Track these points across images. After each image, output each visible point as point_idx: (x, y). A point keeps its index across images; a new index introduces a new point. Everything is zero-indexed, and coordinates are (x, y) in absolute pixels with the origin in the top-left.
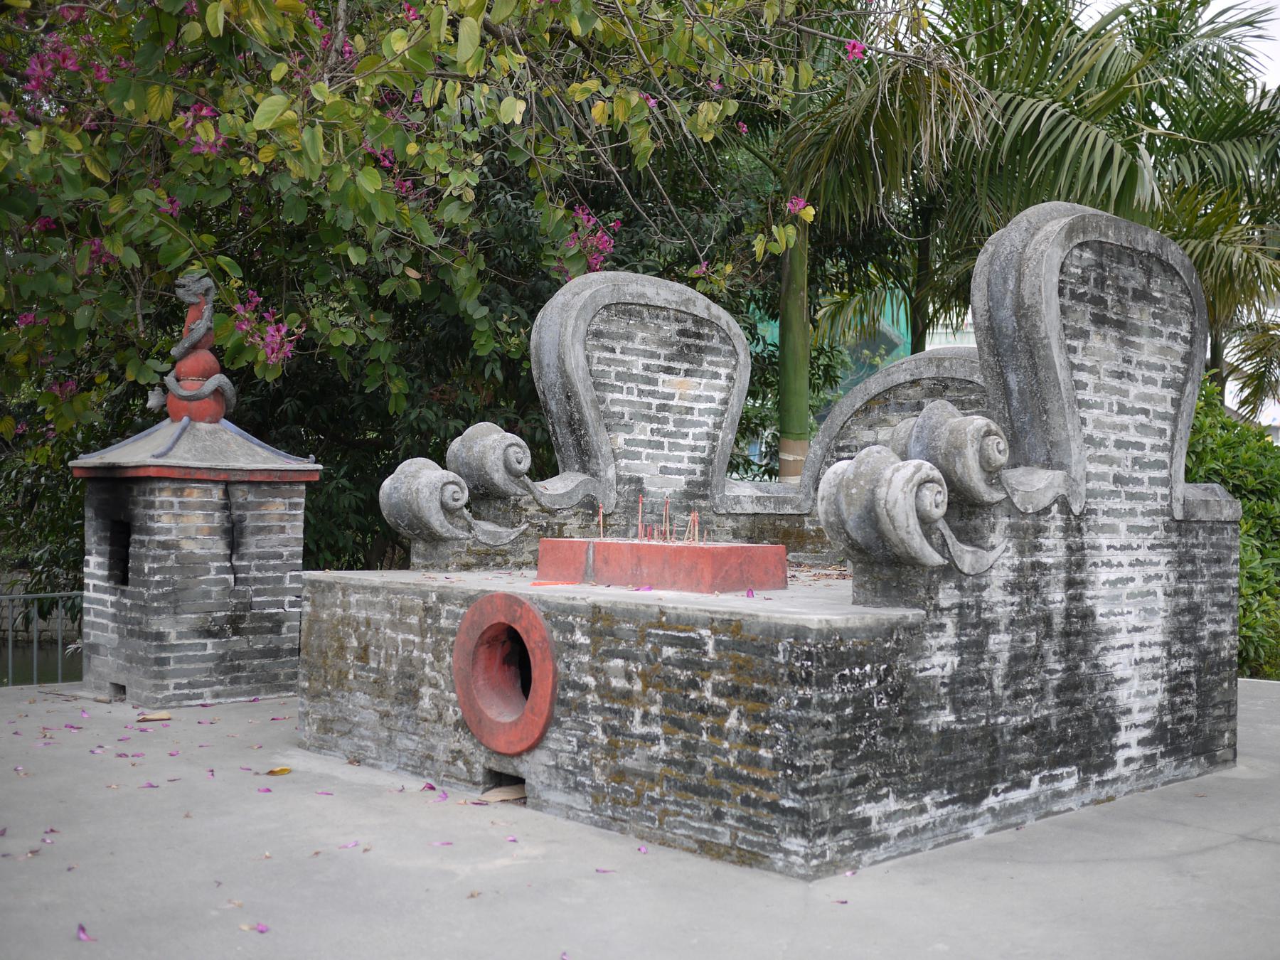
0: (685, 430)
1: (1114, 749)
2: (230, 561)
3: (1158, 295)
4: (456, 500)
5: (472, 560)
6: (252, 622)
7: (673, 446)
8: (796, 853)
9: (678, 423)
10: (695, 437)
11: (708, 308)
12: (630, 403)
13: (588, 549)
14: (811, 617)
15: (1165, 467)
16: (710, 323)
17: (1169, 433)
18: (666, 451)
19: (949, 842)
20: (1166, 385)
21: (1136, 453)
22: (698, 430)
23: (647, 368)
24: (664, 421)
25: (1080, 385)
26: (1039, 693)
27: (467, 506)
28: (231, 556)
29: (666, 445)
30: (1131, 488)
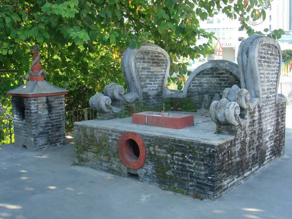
0: (157, 80)
1: (265, 157)
2: (49, 115)
3: (274, 54)
4: (109, 103)
5: (112, 117)
6: (46, 118)
7: (154, 84)
8: (211, 195)
9: (155, 78)
10: (159, 81)
11: (161, 50)
12: (145, 74)
13: (145, 117)
14: (215, 142)
15: (275, 93)
16: (161, 53)
17: (275, 85)
18: (153, 85)
19: (238, 185)
20: (275, 74)
21: (270, 91)
22: (159, 79)
23: (148, 66)
24: (152, 78)
25: (261, 78)
26: (253, 149)
27: (111, 104)
28: (49, 114)
29: (153, 84)
30: (270, 99)
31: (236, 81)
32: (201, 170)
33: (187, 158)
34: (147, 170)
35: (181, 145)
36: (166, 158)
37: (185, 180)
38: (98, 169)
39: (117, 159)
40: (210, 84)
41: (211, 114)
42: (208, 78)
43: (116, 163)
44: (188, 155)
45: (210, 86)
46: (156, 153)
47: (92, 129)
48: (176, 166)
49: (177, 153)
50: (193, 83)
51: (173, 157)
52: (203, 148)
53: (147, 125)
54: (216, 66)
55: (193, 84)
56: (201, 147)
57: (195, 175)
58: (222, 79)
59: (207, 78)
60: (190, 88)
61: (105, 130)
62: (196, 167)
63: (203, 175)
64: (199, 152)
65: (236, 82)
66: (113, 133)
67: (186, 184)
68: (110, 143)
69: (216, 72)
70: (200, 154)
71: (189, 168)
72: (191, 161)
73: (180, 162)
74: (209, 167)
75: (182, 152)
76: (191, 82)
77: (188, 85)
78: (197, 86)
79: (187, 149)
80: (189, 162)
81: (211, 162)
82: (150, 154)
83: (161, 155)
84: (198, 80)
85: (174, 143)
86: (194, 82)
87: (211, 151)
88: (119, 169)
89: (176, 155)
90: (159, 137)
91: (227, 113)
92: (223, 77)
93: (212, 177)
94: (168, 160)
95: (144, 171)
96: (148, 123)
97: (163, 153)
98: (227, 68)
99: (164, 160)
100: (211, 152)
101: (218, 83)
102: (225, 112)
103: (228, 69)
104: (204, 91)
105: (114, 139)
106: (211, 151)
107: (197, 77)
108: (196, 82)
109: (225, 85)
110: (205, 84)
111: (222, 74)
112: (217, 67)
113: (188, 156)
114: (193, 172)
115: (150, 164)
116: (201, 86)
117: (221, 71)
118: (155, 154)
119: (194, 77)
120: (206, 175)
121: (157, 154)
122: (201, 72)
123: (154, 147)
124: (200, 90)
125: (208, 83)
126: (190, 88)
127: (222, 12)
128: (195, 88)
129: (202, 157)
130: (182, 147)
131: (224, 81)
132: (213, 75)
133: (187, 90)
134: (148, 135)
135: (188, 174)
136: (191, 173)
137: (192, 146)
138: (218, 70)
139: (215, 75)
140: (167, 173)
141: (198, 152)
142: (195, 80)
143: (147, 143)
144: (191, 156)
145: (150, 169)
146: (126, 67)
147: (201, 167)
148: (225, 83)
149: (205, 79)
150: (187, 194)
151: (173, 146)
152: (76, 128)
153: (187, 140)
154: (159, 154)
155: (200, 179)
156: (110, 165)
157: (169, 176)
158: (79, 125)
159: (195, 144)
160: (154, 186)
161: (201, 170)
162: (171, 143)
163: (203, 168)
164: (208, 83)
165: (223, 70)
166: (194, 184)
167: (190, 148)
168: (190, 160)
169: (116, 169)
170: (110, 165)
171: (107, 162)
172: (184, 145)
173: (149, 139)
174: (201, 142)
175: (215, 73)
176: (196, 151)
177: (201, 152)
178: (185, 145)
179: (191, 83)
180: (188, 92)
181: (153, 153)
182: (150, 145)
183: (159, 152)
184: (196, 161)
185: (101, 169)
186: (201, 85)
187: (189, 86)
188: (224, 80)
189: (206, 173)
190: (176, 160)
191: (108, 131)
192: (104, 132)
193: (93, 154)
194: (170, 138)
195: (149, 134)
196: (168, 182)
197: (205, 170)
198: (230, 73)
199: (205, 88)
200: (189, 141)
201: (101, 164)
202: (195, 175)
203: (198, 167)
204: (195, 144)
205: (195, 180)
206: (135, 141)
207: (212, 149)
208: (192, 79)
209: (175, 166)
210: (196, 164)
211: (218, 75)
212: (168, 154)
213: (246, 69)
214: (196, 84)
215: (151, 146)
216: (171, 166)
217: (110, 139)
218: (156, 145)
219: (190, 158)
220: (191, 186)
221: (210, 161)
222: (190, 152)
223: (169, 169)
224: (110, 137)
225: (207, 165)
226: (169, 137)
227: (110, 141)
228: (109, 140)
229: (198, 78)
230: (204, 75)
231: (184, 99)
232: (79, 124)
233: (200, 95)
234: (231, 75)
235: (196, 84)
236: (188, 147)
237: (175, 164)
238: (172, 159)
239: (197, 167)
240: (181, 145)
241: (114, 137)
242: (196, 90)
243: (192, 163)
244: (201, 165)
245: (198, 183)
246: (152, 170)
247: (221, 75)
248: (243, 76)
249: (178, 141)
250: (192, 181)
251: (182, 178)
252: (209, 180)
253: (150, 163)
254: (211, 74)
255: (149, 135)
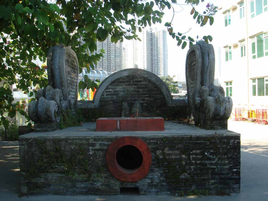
31: (155, 88)
32: (225, 165)
33: (207, 155)
34: (152, 179)
35: (199, 142)
36: (181, 159)
37: (204, 180)
38: (67, 193)
39: (102, 175)
40: (126, 92)
41: (211, 109)
42: (124, 86)
43: (103, 180)
44: (209, 151)
45: (127, 94)
46: (166, 157)
47: (56, 141)
48: (193, 166)
49: (194, 152)
50: (106, 92)
51: (189, 157)
52: (226, 141)
53: (120, 131)
54: (133, 74)
55: (106, 93)
56: (223, 140)
57: (217, 171)
58: (140, 86)
59: (123, 86)
60: (103, 97)
61: (81, 140)
62: (218, 163)
63: (226, 169)
64: (222, 146)
65: (155, 89)
66: (96, 142)
67: (207, 184)
68: (92, 155)
69: (133, 80)
70: (223, 148)
71: (210, 165)
72: (213, 157)
73: (198, 160)
74: (233, 159)
75: (201, 150)
76: (104, 91)
77: (101, 94)
78: (112, 95)
79: (207, 145)
80: (210, 159)
81: (236, 153)
82: (157, 158)
83: (173, 157)
84: (112, 89)
85: (191, 141)
86: (108, 90)
87: (236, 142)
88: (107, 187)
89: (193, 154)
90: (170, 137)
91: (228, 106)
92: (141, 85)
93: (237, 169)
94: (182, 162)
95: (148, 181)
96: (121, 128)
97: (176, 155)
98: (145, 76)
99: (177, 162)
100: (235, 144)
101: (135, 91)
102: (227, 106)
103: (147, 76)
104: (120, 99)
105: (98, 150)
106: (236, 142)
107: (112, 86)
108: (111, 90)
109: (143, 93)
110: (121, 92)
111: (140, 81)
112: (134, 75)
113: (209, 153)
114: (215, 169)
115: (157, 171)
116: (116, 95)
117: (139, 79)
118: (164, 157)
119: (108, 86)
120: (231, 169)
121: (167, 157)
122: (116, 80)
123: (163, 150)
124: (115, 99)
125: (124, 91)
126: (103, 97)
127: (194, 18)
128: (110, 97)
129: (225, 151)
130: (200, 144)
131: (141, 89)
132: (130, 83)
133: (99, 99)
134: (154, 137)
135: (209, 172)
136: (213, 170)
137: (213, 141)
138: (135, 78)
139: (132, 83)
140: (181, 177)
141: (220, 146)
142: (109, 89)
143: (152, 147)
144: (212, 152)
145: (156, 176)
146: (57, 69)
147: (224, 161)
148: (143, 91)
149: (121, 87)
150: (210, 194)
151: (190, 145)
152: (24, 143)
153: (207, 136)
154: (171, 157)
155: (224, 174)
156: (91, 184)
157: (183, 179)
158: (30, 139)
159: (217, 138)
160: (163, 195)
161: (225, 165)
162: (187, 141)
163: (226, 162)
164: (124, 91)
165: (140, 78)
166: (216, 181)
167: (211, 143)
168: (211, 156)
169: (101, 187)
170: (91, 184)
171: (86, 181)
172: (203, 141)
173: (155, 141)
174: (223, 135)
175: (132, 81)
176: (218, 146)
177: (224, 146)
178: (204, 142)
179: (105, 92)
180: (101, 101)
181: (161, 157)
182: (154, 150)
183: (169, 155)
184: (219, 156)
185: (74, 192)
186: (116, 93)
187: (102, 95)
188: (143, 88)
189: (231, 166)
190: (193, 160)
191: (88, 140)
192: (78, 142)
193: (59, 174)
194: (184, 136)
195: (155, 136)
196: (183, 187)
197: (229, 163)
198: (148, 80)
199: (121, 96)
200: (209, 136)
201: (74, 186)
202: (218, 170)
203: (221, 162)
204: (217, 138)
205: (217, 177)
206: (135, 146)
207: (236, 140)
208: (106, 87)
209: (192, 167)
210: (219, 159)
211: (135, 83)
212: (183, 154)
213: (207, 71)
214: (110, 93)
215: (158, 149)
216: (187, 167)
217: (91, 150)
218: (166, 147)
219: (211, 154)
220: (213, 184)
221: (235, 153)
222: (211, 148)
223: (184, 171)
224: (90, 148)
225: (231, 157)
226: (184, 135)
227: (91, 153)
228: (89, 152)
229: (113, 87)
230: (119, 84)
231: (95, 109)
232: (30, 138)
233: (115, 104)
234: (149, 82)
235: (110, 93)
236: (209, 142)
237: (192, 164)
238: (188, 160)
239: (220, 162)
240: (199, 142)
241: (97, 147)
242: (110, 99)
243: (214, 159)
244: (224, 159)
245: (221, 179)
246: (160, 177)
247: (139, 83)
248: (199, 78)
249: (195, 138)
250: (213, 179)
251: (202, 178)
252: (234, 172)
253: (157, 170)
254: (127, 82)
255: (156, 137)
